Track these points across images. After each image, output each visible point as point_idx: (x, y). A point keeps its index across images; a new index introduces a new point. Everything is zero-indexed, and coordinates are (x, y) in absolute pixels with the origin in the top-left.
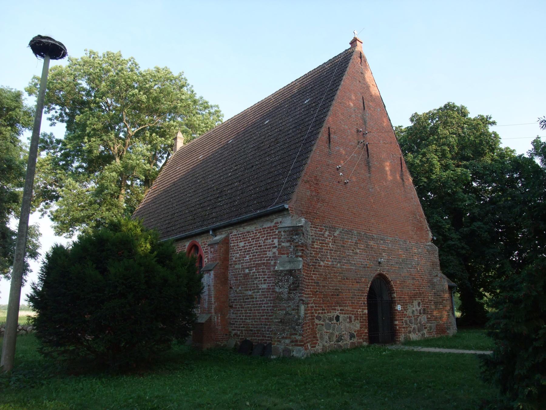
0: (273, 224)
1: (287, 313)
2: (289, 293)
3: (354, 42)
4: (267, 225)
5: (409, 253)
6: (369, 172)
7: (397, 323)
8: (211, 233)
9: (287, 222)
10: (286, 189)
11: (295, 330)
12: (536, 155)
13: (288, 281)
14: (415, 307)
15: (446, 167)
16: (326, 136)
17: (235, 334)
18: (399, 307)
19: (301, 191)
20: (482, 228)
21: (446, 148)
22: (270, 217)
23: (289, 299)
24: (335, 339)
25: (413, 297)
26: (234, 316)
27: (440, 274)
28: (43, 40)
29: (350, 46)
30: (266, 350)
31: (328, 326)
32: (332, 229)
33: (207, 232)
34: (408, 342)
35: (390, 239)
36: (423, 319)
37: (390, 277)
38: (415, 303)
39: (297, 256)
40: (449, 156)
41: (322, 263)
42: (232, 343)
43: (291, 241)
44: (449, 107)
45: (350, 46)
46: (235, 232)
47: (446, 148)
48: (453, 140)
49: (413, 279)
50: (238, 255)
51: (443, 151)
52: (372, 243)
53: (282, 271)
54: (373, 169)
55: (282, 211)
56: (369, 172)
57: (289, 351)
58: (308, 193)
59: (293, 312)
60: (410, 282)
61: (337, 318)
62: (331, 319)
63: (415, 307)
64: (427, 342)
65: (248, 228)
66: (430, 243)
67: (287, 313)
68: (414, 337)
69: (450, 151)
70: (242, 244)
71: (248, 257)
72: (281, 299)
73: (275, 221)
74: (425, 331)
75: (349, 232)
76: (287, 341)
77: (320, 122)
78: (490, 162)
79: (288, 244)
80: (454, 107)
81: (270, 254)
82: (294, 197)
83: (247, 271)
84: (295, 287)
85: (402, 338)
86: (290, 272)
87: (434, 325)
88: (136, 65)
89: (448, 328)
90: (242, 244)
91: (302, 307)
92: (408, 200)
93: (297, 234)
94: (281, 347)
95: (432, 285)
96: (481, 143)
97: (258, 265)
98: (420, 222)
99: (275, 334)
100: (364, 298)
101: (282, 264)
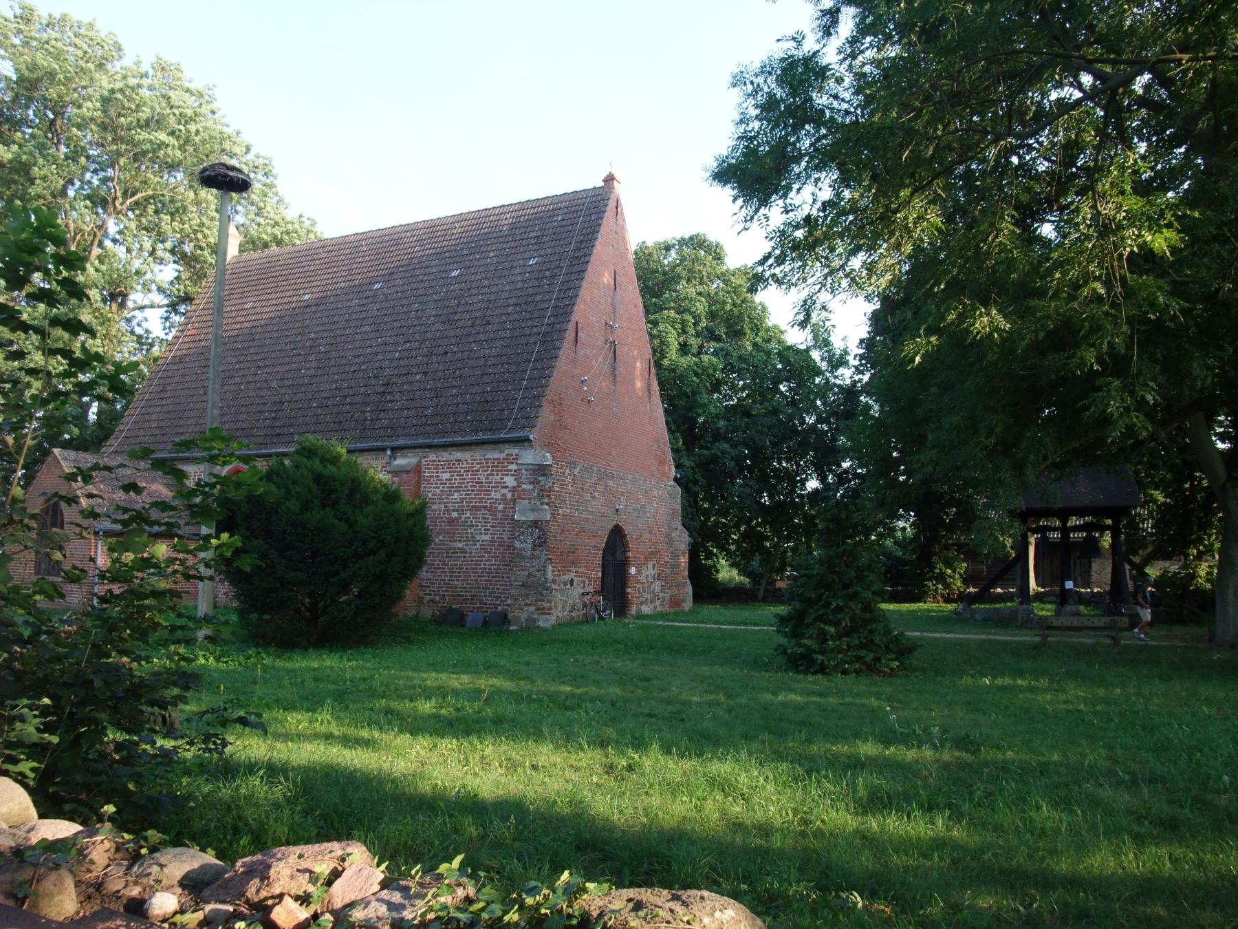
0: (503, 456)
1: (530, 575)
2: (533, 550)
3: (610, 179)
4: (493, 455)
5: (647, 496)
6: (614, 382)
7: (629, 590)
8: (389, 452)
9: (529, 457)
10: (521, 409)
11: (542, 595)
12: (814, 347)
13: (532, 534)
14: (649, 571)
15: (684, 348)
16: (573, 335)
17: (431, 600)
18: (633, 570)
19: (546, 415)
20: (729, 453)
21: (689, 318)
22: (501, 446)
23: (533, 557)
24: (568, 608)
25: (649, 557)
26: (429, 575)
27: (681, 527)
28: (231, 173)
29: (602, 184)
30: (504, 619)
31: (562, 592)
32: (573, 465)
33: (383, 449)
34: (640, 616)
35: (630, 477)
36: (657, 586)
37: (627, 530)
38: (650, 565)
39: (542, 504)
40: (692, 331)
41: (561, 512)
42: (428, 612)
43: (535, 483)
44: (697, 242)
45: (602, 184)
46: (432, 456)
47: (689, 318)
48: (701, 307)
49: (651, 532)
50: (438, 491)
51: (683, 322)
52: (611, 483)
53: (524, 522)
54: (618, 379)
55: (523, 441)
56: (614, 382)
57: (535, 620)
58: (552, 418)
59: (539, 574)
60: (647, 536)
61: (572, 581)
62: (565, 584)
63: (649, 571)
64: (662, 616)
65: (458, 455)
66: (672, 483)
67: (530, 575)
68: (646, 610)
69: (695, 324)
70: (446, 476)
71: (456, 495)
72: (523, 557)
73: (507, 452)
74: (658, 603)
75: (589, 469)
76: (532, 609)
77: (564, 311)
78: (750, 348)
79: (531, 487)
80: (705, 241)
81: (496, 495)
82: (539, 423)
83: (455, 515)
84: (541, 542)
85: (633, 611)
86: (535, 524)
87: (667, 595)
88: (120, 50)
89: (684, 601)
90: (446, 476)
91: (550, 568)
92: (650, 418)
93: (543, 475)
94: (523, 616)
95: (671, 541)
96: (740, 317)
97: (474, 509)
98: (664, 452)
99: (516, 600)
100: (599, 558)
101: (523, 512)
